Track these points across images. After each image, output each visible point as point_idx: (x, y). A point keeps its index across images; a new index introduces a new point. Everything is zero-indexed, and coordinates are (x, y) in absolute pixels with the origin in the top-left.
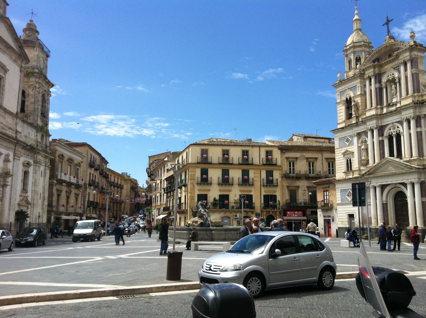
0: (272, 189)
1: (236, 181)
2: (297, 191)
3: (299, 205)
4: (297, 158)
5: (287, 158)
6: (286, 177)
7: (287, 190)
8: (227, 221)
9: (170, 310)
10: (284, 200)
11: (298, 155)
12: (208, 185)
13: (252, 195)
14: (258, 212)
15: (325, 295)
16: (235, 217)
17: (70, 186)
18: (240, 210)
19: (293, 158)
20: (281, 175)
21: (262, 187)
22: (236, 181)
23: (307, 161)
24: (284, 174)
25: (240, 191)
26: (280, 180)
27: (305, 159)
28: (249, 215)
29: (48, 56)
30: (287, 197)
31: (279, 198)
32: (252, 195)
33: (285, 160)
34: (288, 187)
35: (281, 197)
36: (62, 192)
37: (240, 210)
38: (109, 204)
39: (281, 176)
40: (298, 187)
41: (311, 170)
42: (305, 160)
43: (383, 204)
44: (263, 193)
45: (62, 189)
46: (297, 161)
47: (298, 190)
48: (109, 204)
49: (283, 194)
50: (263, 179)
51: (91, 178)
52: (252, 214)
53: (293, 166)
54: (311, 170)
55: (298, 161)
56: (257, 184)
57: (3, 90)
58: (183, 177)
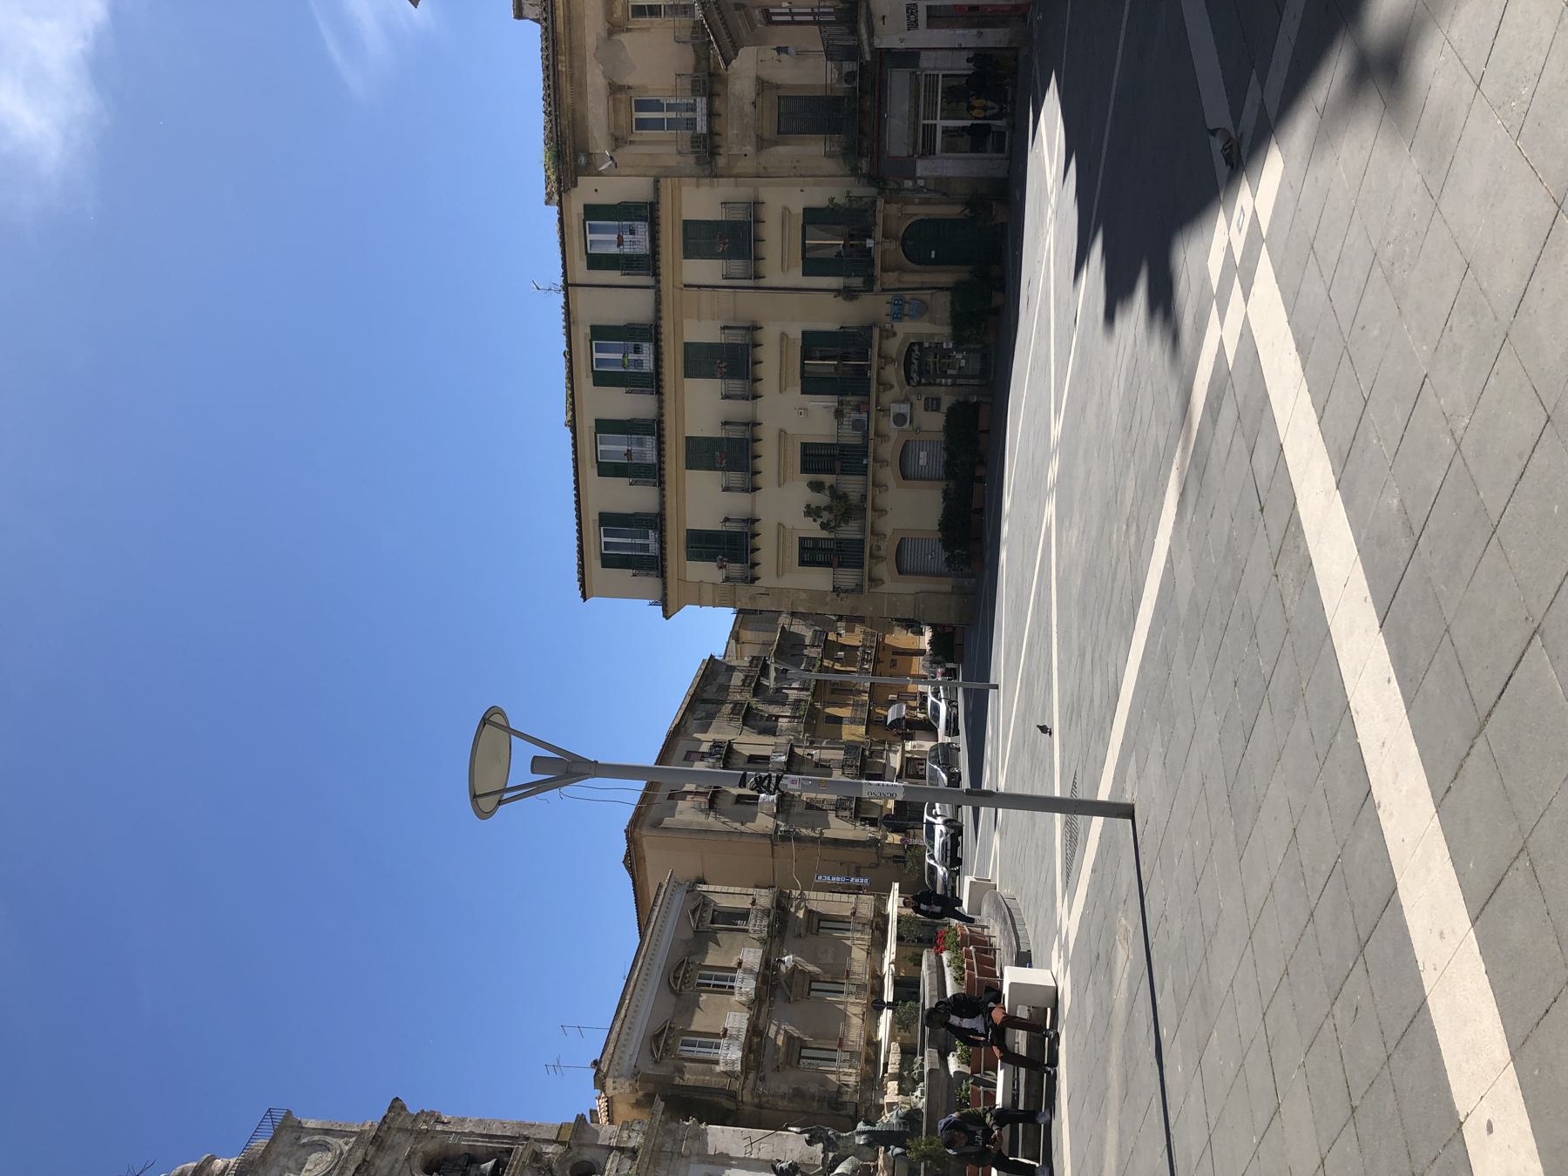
0: (771, 231)
1: (739, 504)
2: (782, 93)
3: (857, 84)
4: (615, 89)
5: (618, 141)
8: (923, 455)
9: (1335, 580)
11: (595, 81)
14: (887, 308)
15: (1180, 288)
17: (831, 242)
19: (614, 108)
21: (763, 283)
22: (739, 504)
23: (628, 30)
24: (699, 162)
27: (616, 37)
32: (804, 333)
38: (994, 129)
39: (707, 181)
40: (762, 85)
41: (672, 115)
42: (624, 38)
44: (796, 277)
46: (629, 88)
47: (778, 87)
48: (994, 129)
50: (726, 278)
52: (895, 334)
54: (672, 115)
56: (750, 305)
58: (723, 386)
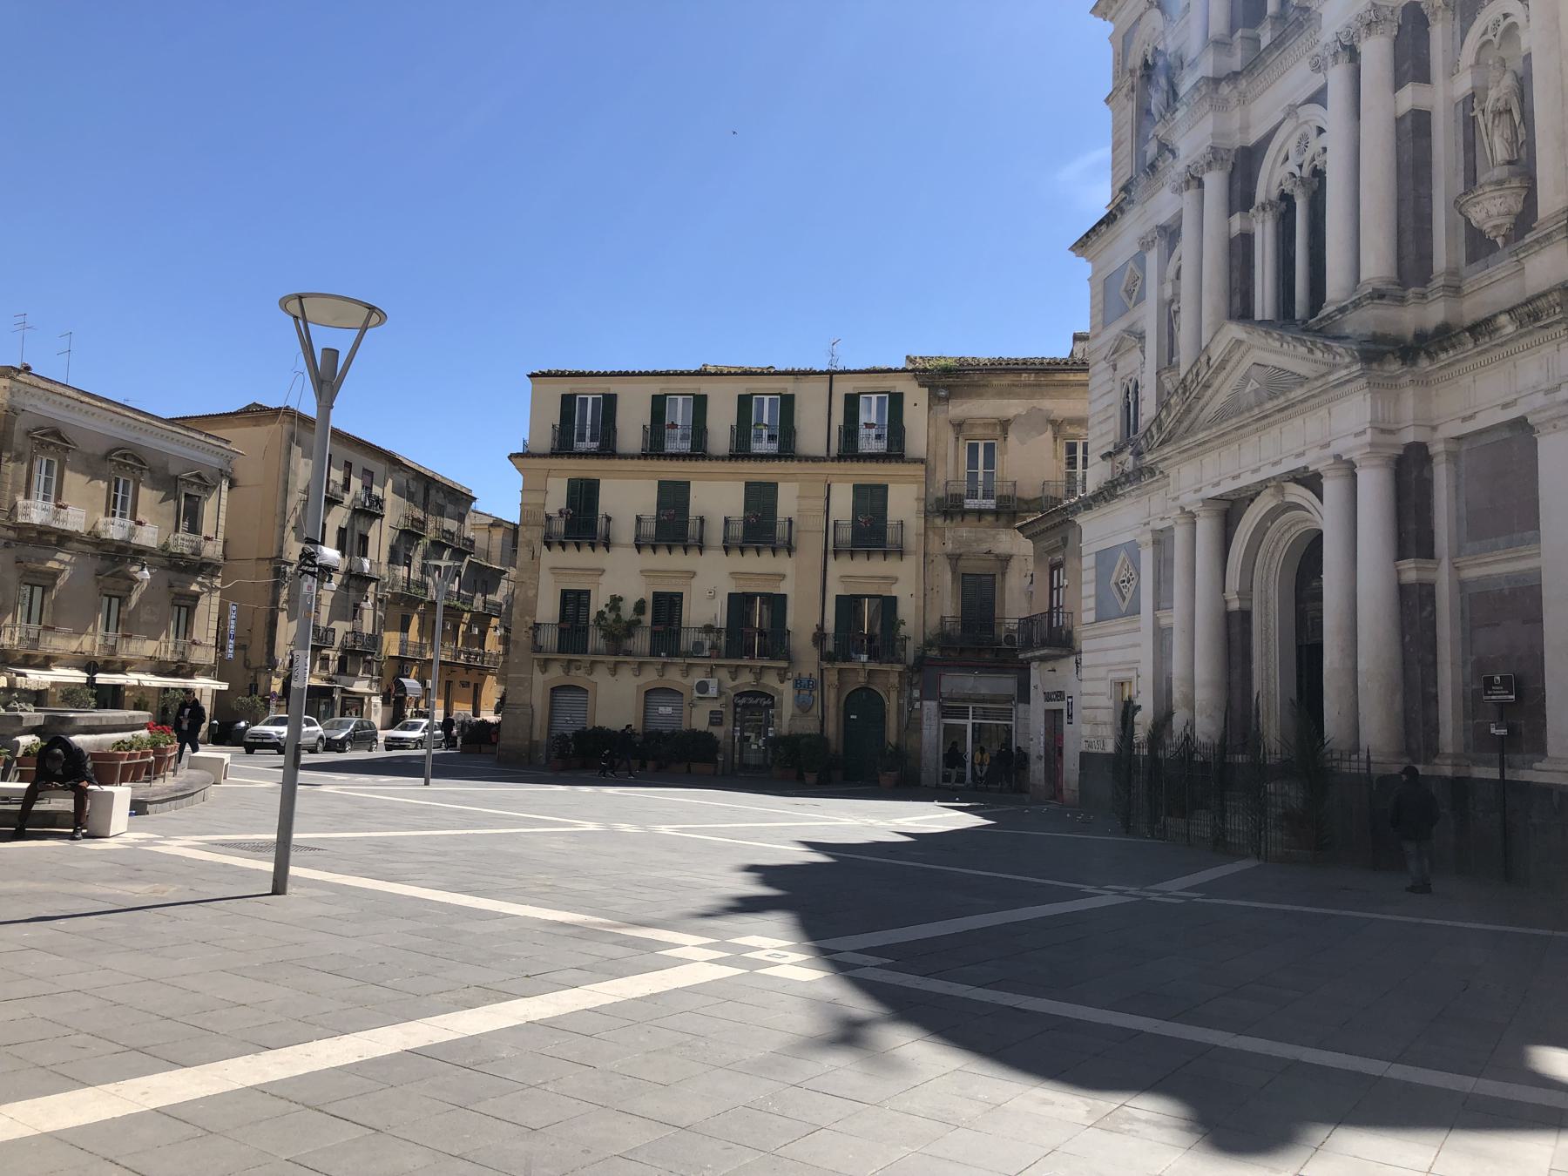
1: (624, 531)
2: (998, 577)
4: (1005, 425)
5: (959, 426)
6: (947, 508)
7: (948, 576)
10: (933, 621)
11: (1012, 407)
12: (564, 549)
13: (784, 596)
16: (699, 692)
18: (974, 721)
19: (988, 424)
20: (922, 504)
21: (831, 557)
22: (624, 531)
25: (734, 575)
26: (914, 523)
28: (766, 686)
29: (27, 369)
30: (948, 606)
31: (907, 610)
32: (784, 596)
33: (950, 435)
34: (954, 559)
35: (916, 607)
36: (1473, 62)
37: (974, 721)
42: (1049, 434)
43: (1228, 616)
44: (835, 589)
45: (1288, 175)
47: (1003, 574)
49: (927, 593)
51: (1451, 294)
52: (782, 682)
53: (989, 463)
55: (1011, 437)
56: (811, 546)
57: (865, 1074)
